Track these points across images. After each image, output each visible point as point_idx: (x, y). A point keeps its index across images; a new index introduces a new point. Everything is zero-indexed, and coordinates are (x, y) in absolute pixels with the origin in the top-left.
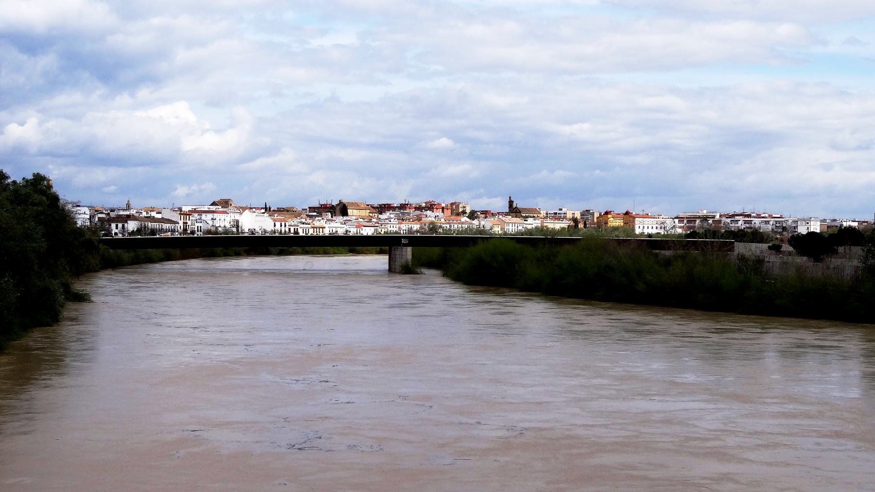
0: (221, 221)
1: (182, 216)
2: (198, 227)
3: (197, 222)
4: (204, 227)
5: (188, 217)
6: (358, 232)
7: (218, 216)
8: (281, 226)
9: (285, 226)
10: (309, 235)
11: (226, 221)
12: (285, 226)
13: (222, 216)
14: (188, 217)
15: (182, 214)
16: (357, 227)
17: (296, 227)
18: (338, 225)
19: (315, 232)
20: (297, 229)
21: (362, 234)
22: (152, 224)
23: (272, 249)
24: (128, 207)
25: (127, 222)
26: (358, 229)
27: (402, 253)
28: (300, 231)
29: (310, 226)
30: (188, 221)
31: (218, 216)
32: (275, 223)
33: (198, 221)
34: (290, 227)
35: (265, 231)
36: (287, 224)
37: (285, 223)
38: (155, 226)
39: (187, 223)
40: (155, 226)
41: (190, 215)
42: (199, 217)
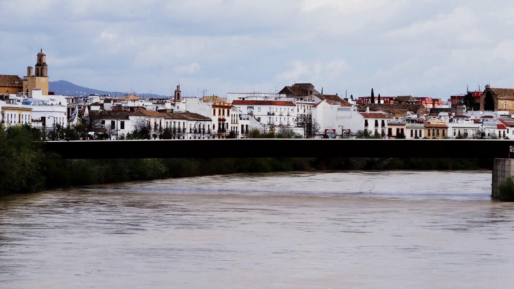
0: (283, 118)
1: (217, 110)
2: (242, 126)
3: (241, 119)
4: (252, 124)
5: (226, 110)
6: (502, 135)
7: (279, 110)
8: (376, 125)
9: (383, 124)
10: (421, 139)
11: (291, 118)
12: (383, 124)
13: (285, 110)
14: (226, 110)
15: (217, 106)
16: (499, 127)
17: (400, 127)
18: (470, 124)
19: (431, 134)
20: (402, 130)
21: (508, 138)
22: (167, 120)
23: (354, 160)
24: (178, 96)
25: (127, 118)
26: (502, 131)
27: (504, 174)
28: (407, 134)
29: (423, 125)
30: (226, 117)
31: (279, 110)
32: (366, 121)
33: (243, 117)
34: (390, 127)
35: (349, 133)
36: (386, 122)
37: (383, 122)
38: (169, 123)
39: (224, 120)
40: (169, 123)
41: (230, 107)
42: (249, 110)
